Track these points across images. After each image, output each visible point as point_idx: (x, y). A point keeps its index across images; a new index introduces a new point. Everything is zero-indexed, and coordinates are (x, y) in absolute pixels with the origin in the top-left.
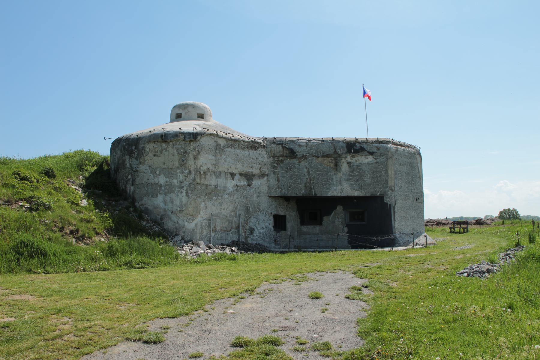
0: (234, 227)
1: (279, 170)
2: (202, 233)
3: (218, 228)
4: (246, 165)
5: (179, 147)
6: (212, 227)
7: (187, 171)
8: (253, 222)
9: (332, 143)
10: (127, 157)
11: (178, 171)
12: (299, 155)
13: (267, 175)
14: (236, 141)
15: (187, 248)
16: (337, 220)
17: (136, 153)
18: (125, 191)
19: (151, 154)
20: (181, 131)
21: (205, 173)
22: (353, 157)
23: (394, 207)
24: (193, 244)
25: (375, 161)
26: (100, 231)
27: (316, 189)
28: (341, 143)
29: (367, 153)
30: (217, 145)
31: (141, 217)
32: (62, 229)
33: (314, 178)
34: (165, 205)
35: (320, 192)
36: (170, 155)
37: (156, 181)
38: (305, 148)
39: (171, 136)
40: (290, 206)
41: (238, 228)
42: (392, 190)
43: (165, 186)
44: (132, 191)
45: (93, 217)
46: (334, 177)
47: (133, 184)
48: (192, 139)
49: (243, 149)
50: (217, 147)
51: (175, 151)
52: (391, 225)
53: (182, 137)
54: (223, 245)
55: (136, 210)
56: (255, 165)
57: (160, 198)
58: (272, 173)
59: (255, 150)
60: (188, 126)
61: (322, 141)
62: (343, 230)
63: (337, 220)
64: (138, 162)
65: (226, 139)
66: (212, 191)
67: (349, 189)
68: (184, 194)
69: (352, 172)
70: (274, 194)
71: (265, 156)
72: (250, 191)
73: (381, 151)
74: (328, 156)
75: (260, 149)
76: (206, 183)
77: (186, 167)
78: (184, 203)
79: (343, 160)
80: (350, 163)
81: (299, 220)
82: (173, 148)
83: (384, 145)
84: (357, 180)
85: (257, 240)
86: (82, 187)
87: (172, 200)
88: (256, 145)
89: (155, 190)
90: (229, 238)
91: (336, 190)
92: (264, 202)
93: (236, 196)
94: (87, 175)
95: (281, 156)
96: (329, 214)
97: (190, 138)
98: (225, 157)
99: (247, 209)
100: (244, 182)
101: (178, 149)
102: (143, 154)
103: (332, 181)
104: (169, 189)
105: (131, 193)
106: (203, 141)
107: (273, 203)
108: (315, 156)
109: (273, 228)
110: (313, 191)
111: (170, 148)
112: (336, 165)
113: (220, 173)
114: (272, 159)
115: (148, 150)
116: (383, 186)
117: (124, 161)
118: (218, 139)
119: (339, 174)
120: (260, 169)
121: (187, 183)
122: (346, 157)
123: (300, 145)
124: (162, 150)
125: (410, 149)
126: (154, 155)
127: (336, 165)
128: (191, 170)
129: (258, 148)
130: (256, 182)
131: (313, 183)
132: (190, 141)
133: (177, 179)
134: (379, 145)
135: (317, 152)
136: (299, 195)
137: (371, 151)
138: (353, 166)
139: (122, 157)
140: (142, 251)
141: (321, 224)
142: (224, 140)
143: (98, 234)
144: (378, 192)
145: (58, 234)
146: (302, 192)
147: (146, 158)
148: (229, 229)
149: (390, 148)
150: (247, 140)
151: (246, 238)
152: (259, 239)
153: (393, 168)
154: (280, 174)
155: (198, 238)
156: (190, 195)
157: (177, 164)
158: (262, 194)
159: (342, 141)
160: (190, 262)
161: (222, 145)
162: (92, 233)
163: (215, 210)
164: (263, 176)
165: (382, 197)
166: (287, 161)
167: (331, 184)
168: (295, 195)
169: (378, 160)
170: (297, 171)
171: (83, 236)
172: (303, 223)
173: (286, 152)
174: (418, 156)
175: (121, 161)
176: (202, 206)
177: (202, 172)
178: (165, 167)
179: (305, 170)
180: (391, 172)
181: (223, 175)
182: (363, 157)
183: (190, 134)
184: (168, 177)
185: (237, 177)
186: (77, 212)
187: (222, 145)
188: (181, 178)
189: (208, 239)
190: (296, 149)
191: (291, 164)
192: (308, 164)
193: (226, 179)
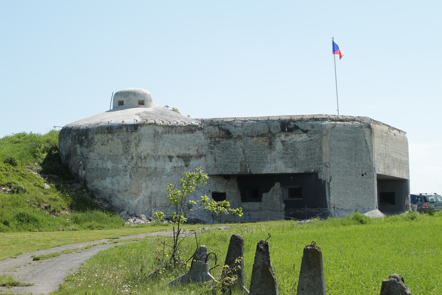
1: (216, 150)
2: (144, 209)
3: (158, 205)
4: (183, 148)
5: (123, 137)
6: (153, 203)
7: (130, 157)
9: (267, 123)
10: (78, 146)
11: (123, 157)
12: (235, 135)
13: (205, 156)
14: (173, 127)
15: (132, 220)
16: (275, 196)
17: (86, 143)
18: (77, 175)
19: (99, 144)
20: (124, 123)
21: (145, 158)
22: (287, 135)
23: (329, 184)
24: (136, 217)
25: (309, 139)
26: (65, 207)
27: (251, 168)
28: (275, 122)
30: (155, 133)
31: (93, 196)
32: (39, 206)
34: (113, 186)
36: (116, 144)
37: (104, 166)
38: (240, 128)
39: (115, 128)
40: (230, 183)
42: (326, 166)
43: (112, 170)
44: (83, 175)
45: (58, 197)
46: (268, 155)
47: (84, 169)
48: (133, 130)
49: (180, 133)
50: (156, 134)
53: (125, 129)
55: (88, 191)
56: (193, 147)
57: (108, 180)
58: (209, 153)
59: (192, 133)
60: (130, 116)
61: (258, 121)
62: (281, 206)
63: (275, 196)
64: (88, 150)
65: (163, 126)
67: (283, 166)
68: (128, 176)
69: (286, 150)
71: (203, 138)
73: (316, 128)
74: (262, 135)
75: (197, 131)
76: (147, 166)
77: (129, 154)
78: (128, 183)
79: (277, 139)
80: (284, 141)
81: (240, 197)
82: (117, 138)
83: (319, 122)
84: (291, 158)
85: (195, 215)
86: (41, 173)
87: (119, 181)
88: (194, 128)
89: (103, 173)
91: (270, 168)
93: (174, 176)
94: (41, 161)
95: (219, 137)
96: (267, 191)
97: (131, 129)
98: (163, 142)
100: (181, 163)
101: (121, 139)
102: (92, 144)
103: (266, 159)
104: (116, 173)
105: (83, 176)
106: (143, 130)
107: (212, 181)
108: (250, 136)
110: (248, 169)
112: (270, 144)
113: (159, 156)
114: (209, 140)
115: (96, 140)
116: (317, 163)
117: (76, 149)
118: (157, 127)
119: (273, 152)
120: (197, 151)
121: (131, 167)
122: (280, 136)
123: (235, 126)
124: (109, 140)
126: (102, 144)
127: (270, 144)
128: (134, 156)
129: (195, 130)
130: (193, 163)
131: (248, 161)
132: (132, 132)
133: (122, 164)
135: (252, 132)
136: (235, 173)
137: (305, 129)
139: (73, 146)
140: (99, 220)
141: (260, 201)
142: (162, 127)
143: (64, 209)
144: (312, 168)
145: (38, 209)
146: (238, 170)
147: (95, 147)
148: (168, 205)
149: (325, 126)
150: (184, 125)
152: (197, 215)
153: (328, 145)
154: (217, 154)
155: (141, 212)
156: (133, 177)
157: (121, 151)
160: (133, 227)
161: (160, 132)
162: (59, 209)
164: (200, 156)
166: (223, 142)
167: (265, 162)
168: (231, 173)
169: (312, 138)
170: (233, 151)
171: (54, 211)
173: (222, 132)
174: (367, 131)
175: (72, 149)
176: (143, 186)
177: (143, 158)
178: (112, 154)
179: (241, 150)
180: (325, 149)
181: (161, 158)
182: (297, 135)
183: (131, 125)
184: (115, 163)
185: (174, 160)
186: (44, 193)
187: (160, 132)
188: (125, 163)
189: (149, 214)
191: (227, 144)
193: (165, 161)
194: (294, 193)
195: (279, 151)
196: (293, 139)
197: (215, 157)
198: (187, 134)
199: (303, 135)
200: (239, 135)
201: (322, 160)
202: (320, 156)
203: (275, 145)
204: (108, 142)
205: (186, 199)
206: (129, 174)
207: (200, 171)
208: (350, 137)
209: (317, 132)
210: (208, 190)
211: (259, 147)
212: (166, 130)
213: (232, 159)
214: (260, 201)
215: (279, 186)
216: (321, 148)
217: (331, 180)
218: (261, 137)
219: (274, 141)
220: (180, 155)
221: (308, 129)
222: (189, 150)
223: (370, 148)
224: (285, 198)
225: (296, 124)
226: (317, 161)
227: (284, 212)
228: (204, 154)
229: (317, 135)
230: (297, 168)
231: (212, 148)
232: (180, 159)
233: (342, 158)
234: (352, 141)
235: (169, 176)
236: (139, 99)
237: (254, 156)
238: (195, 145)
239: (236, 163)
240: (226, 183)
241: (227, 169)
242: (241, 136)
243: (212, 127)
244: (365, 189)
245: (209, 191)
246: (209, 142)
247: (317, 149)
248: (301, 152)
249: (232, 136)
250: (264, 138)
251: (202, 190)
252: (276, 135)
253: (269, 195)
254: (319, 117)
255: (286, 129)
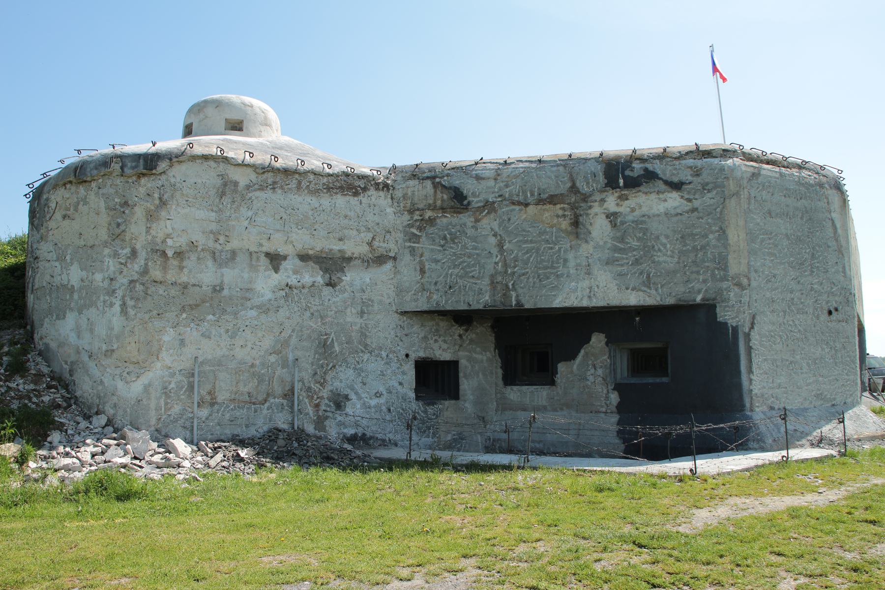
0: (278, 390)
1: (425, 245)
5: (112, 191)
7: (127, 251)
8: (343, 379)
9: (565, 166)
11: (107, 251)
12: (476, 202)
13: (395, 259)
16: (592, 372)
21: (179, 254)
23: (748, 336)
25: (688, 206)
27: (520, 291)
28: (589, 163)
29: (663, 187)
30: (225, 185)
33: (516, 260)
34: (78, 337)
35: (533, 297)
38: (492, 183)
39: (92, 166)
40: (474, 336)
41: (289, 395)
42: (739, 285)
43: (81, 289)
46: (571, 256)
48: (141, 169)
49: (315, 192)
50: (227, 187)
51: (102, 204)
52: (739, 386)
53: (116, 167)
54: (218, 441)
56: (355, 232)
57: (71, 319)
58: (407, 251)
59: (356, 194)
62: (607, 398)
63: (592, 372)
66: (203, 302)
67: (613, 286)
68: (117, 308)
69: (622, 240)
70: (412, 307)
71: (389, 210)
72: (332, 299)
73: (706, 177)
74: (553, 200)
75: (372, 192)
76: (184, 278)
78: (117, 329)
79: (596, 209)
80: (615, 214)
81: (500, 372)
82: (97, 194)
84: (637, 262)
90: (260, 422)
91: (576, 290)
92: (385, 327)
93: (283, 313)
96: (572, 356)
97: (136, 167)
98: (250, 213)
99: (324, 346)
100: (312, 276)
101: (107, 197)
103: (565, 265)
107: (416, 328)
108: (519, 203)
109: (412, 395)
110: (514, 294)
111: (92, 196)
112: (576, 223)
113: (234, 254)
114: (406, 217)
116: (713, 275)
119: (584, 245)
120: (370, 244)
121: (125, 281)
122: (603, 201)
123: (478, 178)
124: (78, 203)
125: (805, 173)
126: (64, 217)
127: (576, 223)
128: (138, 246)
129: (365, 189)
131: (514, 273)
132: (141, 175)
133: (102, 271)
134: (699, 163)
135: (524, 192)
136: (476, 306)
137: (675, 179)
138: (623, 223)
141: (552, 383)
142: (249, 170)
144: (699, 292)
146: (481, 297)
148: (261, 398)
149: (732, 169)
150: (327, 170)
151: (320, 423)
153: (741, 223)
154: (427, 255)
156: (132, 312)
157: (103, 234)
158: (376, 307)
159: (596, 160)
163: (209, 349)
164: (380, 260)
165: (709, 308)
166: (445, 220)
167: (562, 275)
168: (465, 307)
169: (696, 203)
170: (470, 244)
172: (510, 379)
173: (446, 196)
174: (833, 194)
176: (166, 338)
177: (170, 253)
179: (493, 240)
180: (736, 235)
181: (241, 258)
182: (653, 196)
184: (85, 269)
188: (112, 268)
189: (188, 424)
190: (468, 187)
192: (500, 226)
193: (253, 268)
194: (645, 362)
195: (601, 243)
196: (640, 207)
197: (421, 263)
198: (339, 196)
199: (670, 195)
200: (487, 201)
201: (726, 266)
202: (720, 254)
203: (588, 226)
204: (76, 210)
205: (328, 378)
206: (118, 303)
207: (379, 295)
208: (797, 209)
209: (710, 187)
210: (403, 353)
211: (545, 232)
212: (265, 181)
213: (468, 266)
214: (552, 383)
215: (603, 343)
216: (724, 232)
217: (753, 324)
218: (550, 203)
219: (587, 215)
220: (311, 252)
221: (684, 179)
222: (341, 240)
223: (843, 243)
224: (619, 376)
225: (650, 167)
226: (713, 271)
227: (615, 418)
228: (392, 254)
229: (710, 195)
230: (653, 292)
231: (415, 238)
232: (311, 263)
233: (781, 263)
234: (802, 218)
235: (267, 312)
236: (228, 117)
237: (528, 259)
238: (363, 229)
239: (478, 278)
240: (460, 336)
241: (453, 294)
242: (494, 203)
243: (416, 182)
244: (836, 351)
245: (407, 356)
246: (405, 223)
247: (711, 236)
248: (664, 245)
249: (469, 203)
250: (558, 206)
251: (384, 354)
252: (593, 198)
253: (575, 367)
254: (712, 148)
255: (621, 182)
